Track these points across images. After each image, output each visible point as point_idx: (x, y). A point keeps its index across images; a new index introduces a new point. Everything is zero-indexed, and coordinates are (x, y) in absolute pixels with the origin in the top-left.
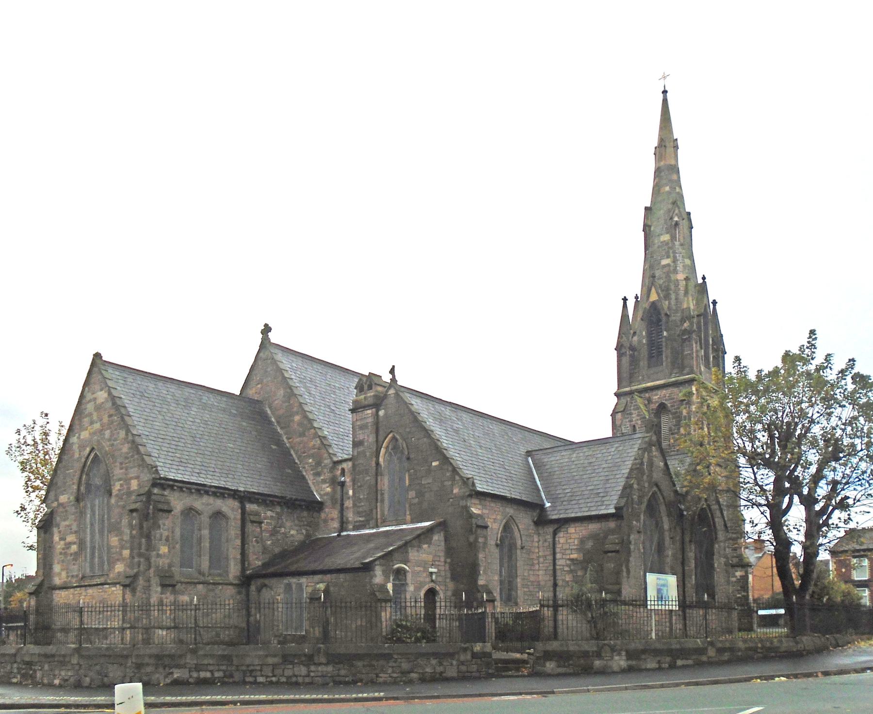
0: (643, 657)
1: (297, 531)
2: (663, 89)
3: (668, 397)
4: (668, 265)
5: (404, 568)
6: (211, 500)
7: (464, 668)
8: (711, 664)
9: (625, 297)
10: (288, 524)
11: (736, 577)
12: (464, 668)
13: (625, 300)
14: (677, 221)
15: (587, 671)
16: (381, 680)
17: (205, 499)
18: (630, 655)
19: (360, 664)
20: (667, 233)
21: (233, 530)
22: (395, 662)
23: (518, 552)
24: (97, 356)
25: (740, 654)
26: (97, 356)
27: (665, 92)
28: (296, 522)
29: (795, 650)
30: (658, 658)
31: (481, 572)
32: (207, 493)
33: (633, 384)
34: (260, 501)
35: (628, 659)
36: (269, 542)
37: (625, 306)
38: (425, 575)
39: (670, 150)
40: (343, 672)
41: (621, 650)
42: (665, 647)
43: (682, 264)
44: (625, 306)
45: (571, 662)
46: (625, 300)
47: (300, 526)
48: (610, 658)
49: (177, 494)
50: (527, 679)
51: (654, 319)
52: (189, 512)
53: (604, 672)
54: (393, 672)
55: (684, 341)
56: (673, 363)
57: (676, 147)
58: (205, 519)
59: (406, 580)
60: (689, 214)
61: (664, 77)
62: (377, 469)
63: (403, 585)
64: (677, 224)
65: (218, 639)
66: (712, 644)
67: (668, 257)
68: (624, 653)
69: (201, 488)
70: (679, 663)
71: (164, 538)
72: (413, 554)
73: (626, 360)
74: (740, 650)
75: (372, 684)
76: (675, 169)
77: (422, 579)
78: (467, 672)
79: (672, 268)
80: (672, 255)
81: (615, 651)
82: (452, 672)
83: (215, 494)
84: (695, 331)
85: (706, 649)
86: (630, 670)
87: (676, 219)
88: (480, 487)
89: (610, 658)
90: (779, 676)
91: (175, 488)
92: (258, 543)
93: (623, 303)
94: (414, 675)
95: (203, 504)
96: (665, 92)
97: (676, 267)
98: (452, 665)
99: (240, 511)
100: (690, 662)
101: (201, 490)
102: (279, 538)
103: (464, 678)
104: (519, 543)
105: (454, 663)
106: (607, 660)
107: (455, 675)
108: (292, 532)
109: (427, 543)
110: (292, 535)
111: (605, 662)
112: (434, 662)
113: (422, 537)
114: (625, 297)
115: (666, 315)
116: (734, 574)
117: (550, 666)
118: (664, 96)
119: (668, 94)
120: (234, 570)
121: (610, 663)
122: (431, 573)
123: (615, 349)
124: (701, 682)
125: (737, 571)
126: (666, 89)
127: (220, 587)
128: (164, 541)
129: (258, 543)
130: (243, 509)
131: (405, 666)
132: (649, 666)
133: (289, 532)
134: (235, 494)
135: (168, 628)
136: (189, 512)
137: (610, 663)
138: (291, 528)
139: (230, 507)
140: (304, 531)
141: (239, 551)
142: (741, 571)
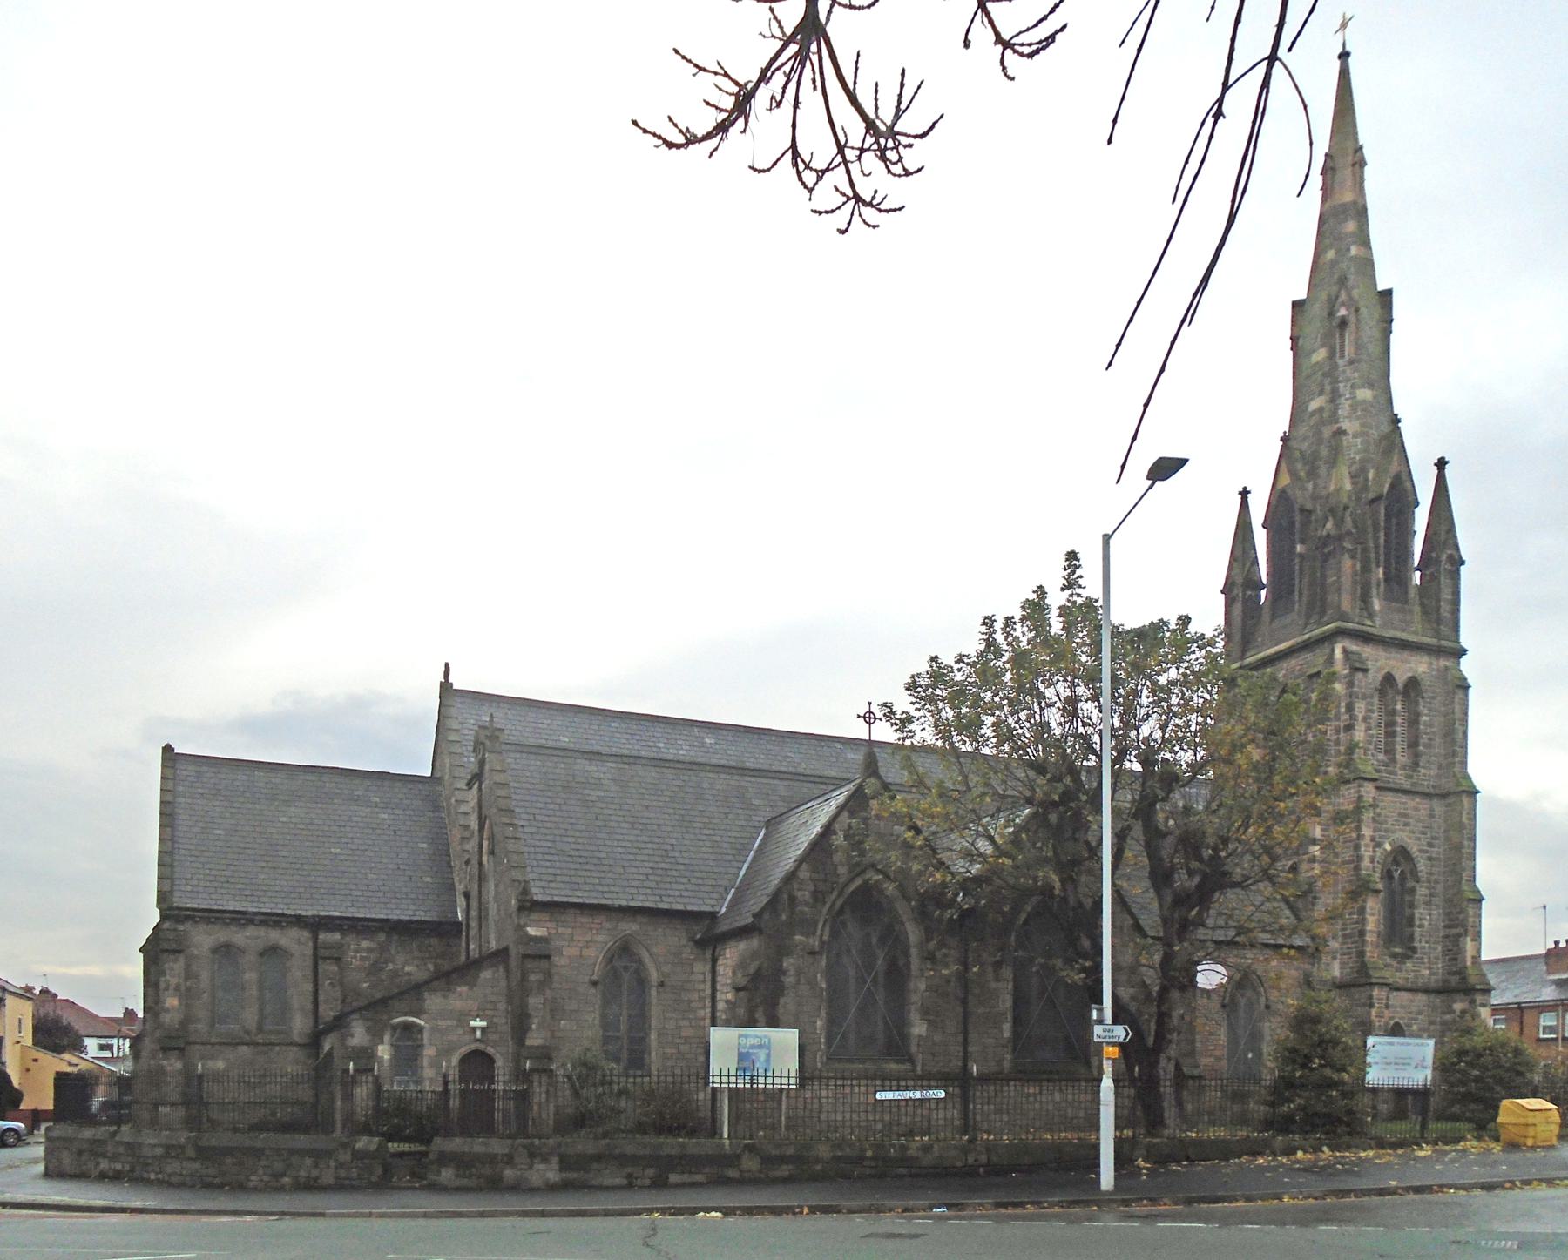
0: (595, 1166)
1: (417, 966)
2: (1340, 50)
3: (1300, 670)
4: (1321, 410)
5: (413, 1021)
6: (262, 931)
7: (343, 1173)
8: (744, 1182)
9: (1245, 488)
10: (400, 958)
11: (1454, 1012)
12: (343, 1173)
13: (1244, 493)
14: (1343, 317)
15: (495, 1185)
16: (251, 1184)
17: (251, 931)
18: (565, 1164)
19: (229, 1160)
20: (1323, 346)
21: (298, 971)
22: (267, 1159)
23: (654, 992)
24: (168, 749)
25: (819, 1167)
26: (168, 749)
27: (1344, 56)
28: (416, 953)
29: (959, 1164)
30: (629, 1170)
31: (534, 1026)
32: (251, 922)
33: (1249, 654)
34: (345, 927)
35: (561, 1170)
36: (365, 985)
37: (1244, 505)
38: (460, 1031)
39: (1346, 174)
40: (212, 1171)
41: (551, 1154)
42: (647, 1152)
43: (1349, 402)
44: (1244, 505)
45: (474, 1170)
46: (1244, 493)
47: (423, 959)
48: (526, 1167)
49: (202, 927)
50: (418, 1192)
51: (1284, 523)
52: (225, 951)
53: (516, 1188)
54: (265, 1174)
55: (1326, 558)
56: (1311, 607)
57: (1361, 163)
58: (251, 957)
59: (422, 1039)
60: (1387, 295)
61: (1344, 25)
62: (480, 871)
63: (419, 1046)
64: (1343, 323)
65: (273, 1119)
66: (750, 1148)
67: (1321, 393)
68: (555, 1160)
69: (239, 916)
70: (674, 1178)
71: (172, 988)
72: (433, 1001)
73: (1238, 609)
74: (818, 1160)
75: (240, 1187)
76: (1360, 212)
77: (455, 1038)
78: (348, 1179)
79: (1326, 415)
80: (1328, 388)
81: (535, 1157)
82: (328, 1178)
83: (263, 923)
84: (1349, 533)
85: (738, 1157)
86: (565, 1187)
87: (1343, 312)
88: (538, 894)
89: (526, 1167)
90: (708, 1210)
91: (198, 919)
92: (334, 987)
93: (1240, 501)
94: (286, 1180)
95: (247, 937)
96: (1344, 56)
97: (1336, 410)
98: (328, 1166)
99: (311, 944)
100: (699, 1178)
101: (241, 919)
102: (384, 977)
103: (340, 1187)
104: (654, 976)
105: (332, 1164)
106: (521, 1169)
107: (331, 1181)
108: (407, 969)
109: (465, 984)
110: (409, 974)
111: (519, 1173)
112: (308, 1161)
113: (454, 976)
114: (1245, 488)
115: (1302, 510)
116: (1450, 1007)
117: (447, 1175)
118: (1341, 64)
119: (1351, 60)
120: (300, 1025)
121: (527, 1174)
122: (474, 1029)
123: (1222, 592)
124: (550, 1211)
125: (1455, 1001)
126: (1348, 48)
127: (277, 1048)
128: (171, 991)
129: (334, 987)
130: (315, 939)
131: (278, 1166)
132: (607, 1182)
133: (403, 968)
134: (299, 921)
135: (173, 1104)
136: (225, 951)
137: (527, 1174)
138: (406, 963)
139: (293, 940)
140: (431, 967)
141: (311, 998)
142: (1462, 1001)
